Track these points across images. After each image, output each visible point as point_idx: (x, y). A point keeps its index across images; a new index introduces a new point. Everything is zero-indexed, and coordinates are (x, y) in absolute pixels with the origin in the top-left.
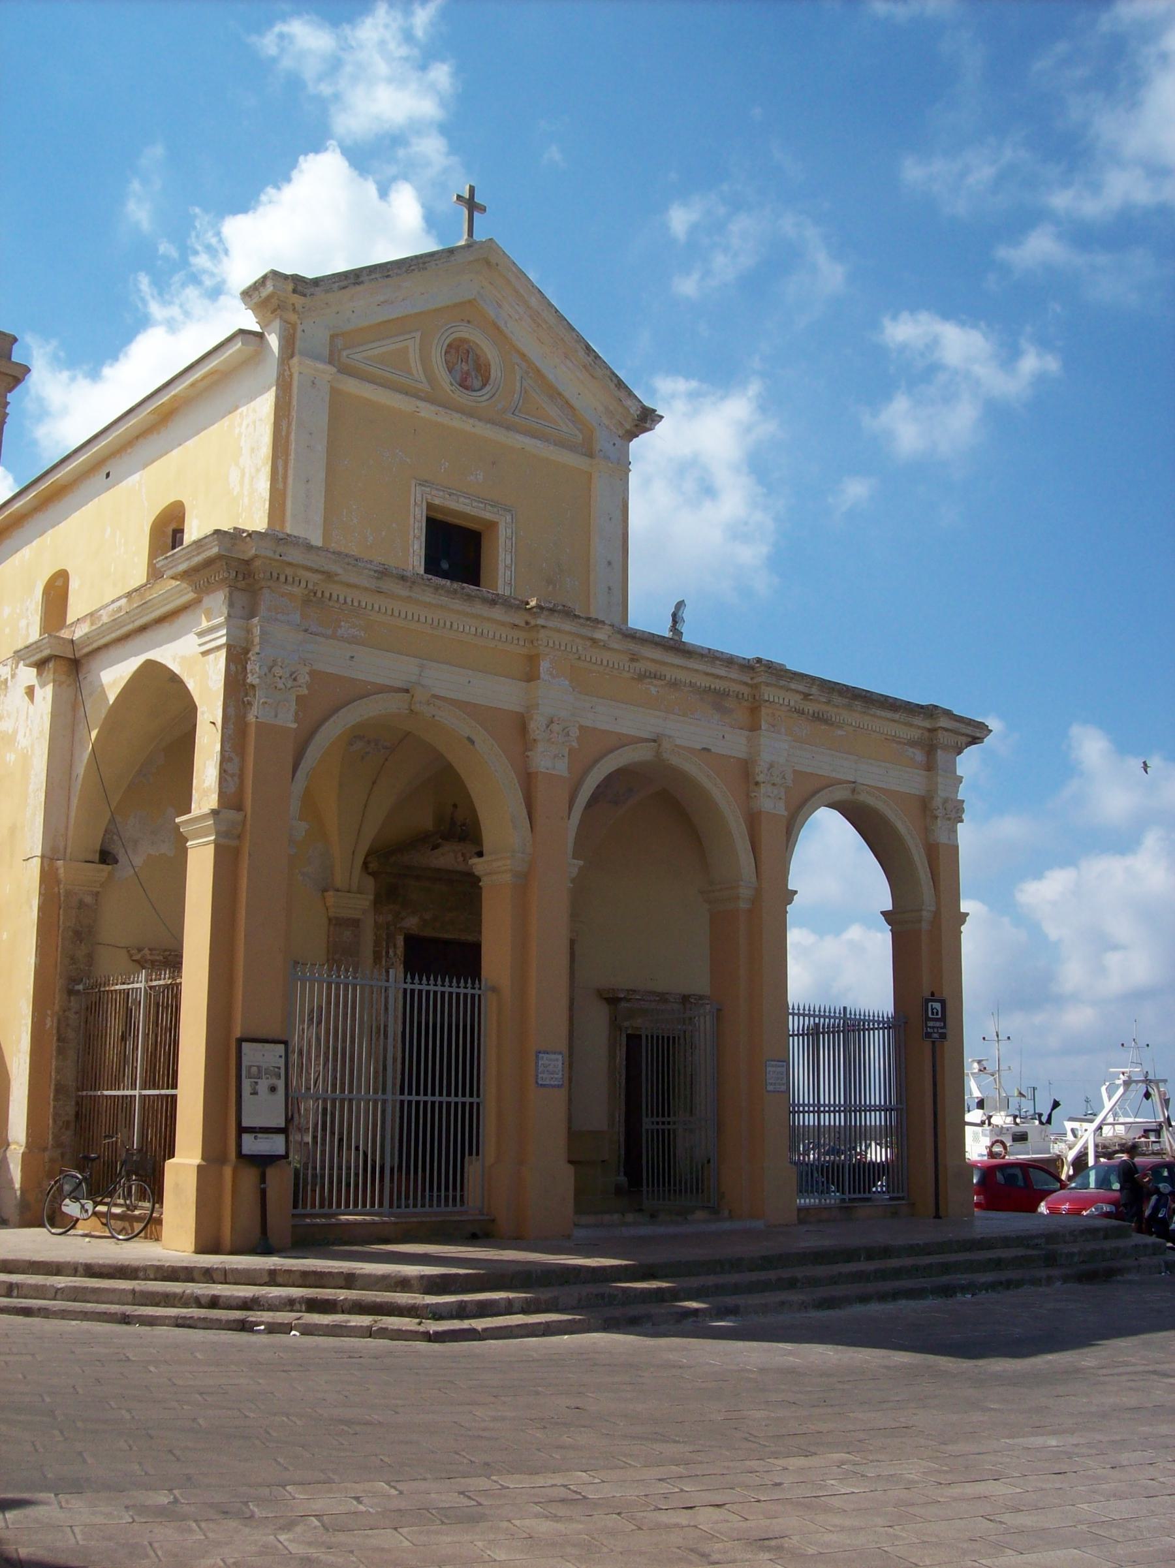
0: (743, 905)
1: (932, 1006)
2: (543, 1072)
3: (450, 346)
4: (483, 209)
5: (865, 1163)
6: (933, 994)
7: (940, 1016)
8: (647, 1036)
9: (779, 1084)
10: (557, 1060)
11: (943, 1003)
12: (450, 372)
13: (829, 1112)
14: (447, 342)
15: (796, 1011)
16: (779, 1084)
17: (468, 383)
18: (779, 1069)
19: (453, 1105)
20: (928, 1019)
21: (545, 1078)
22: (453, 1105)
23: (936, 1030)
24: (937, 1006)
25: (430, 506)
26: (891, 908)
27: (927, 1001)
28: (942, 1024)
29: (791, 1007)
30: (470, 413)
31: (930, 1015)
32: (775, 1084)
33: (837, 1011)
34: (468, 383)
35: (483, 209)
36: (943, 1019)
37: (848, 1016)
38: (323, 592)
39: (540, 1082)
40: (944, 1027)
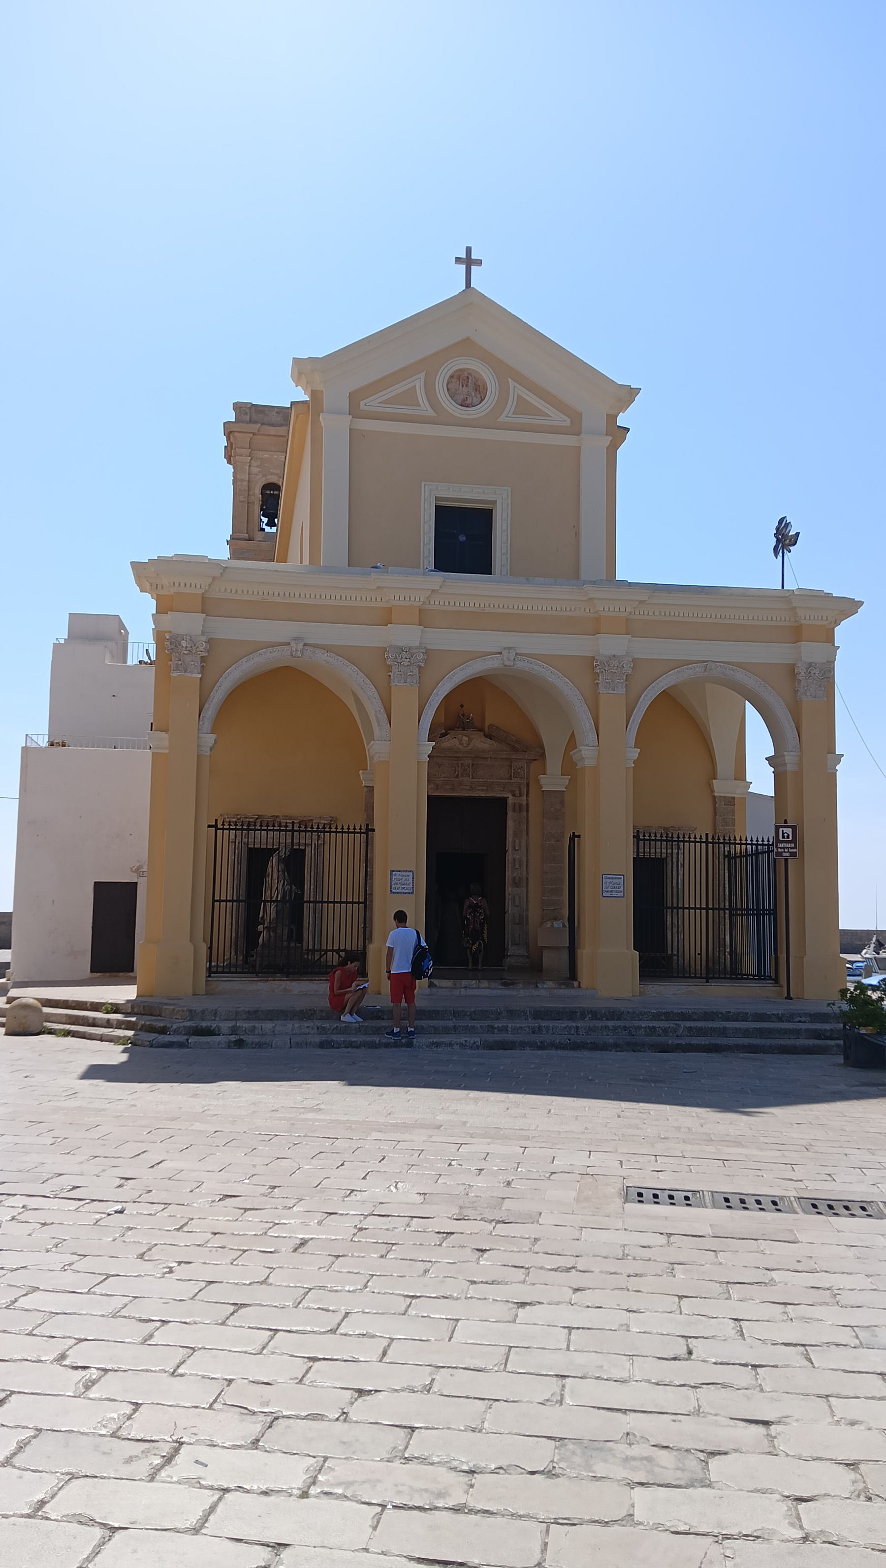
0: (588, 763)
1: (783, 831)
2: (397, 884)
3: (452, 377)
4: (479, 263)
6: (786, 822)
7: (791, 839)
9: (619, 892)
13: (742, 915)
16: (619, 892)
24: (789, 831)
25: (437, 499)
26: (773, 754)
31: (781, 838)
32: (611, 891)
35: (479, 263)
38: (822, 616)
39: (393, 891)
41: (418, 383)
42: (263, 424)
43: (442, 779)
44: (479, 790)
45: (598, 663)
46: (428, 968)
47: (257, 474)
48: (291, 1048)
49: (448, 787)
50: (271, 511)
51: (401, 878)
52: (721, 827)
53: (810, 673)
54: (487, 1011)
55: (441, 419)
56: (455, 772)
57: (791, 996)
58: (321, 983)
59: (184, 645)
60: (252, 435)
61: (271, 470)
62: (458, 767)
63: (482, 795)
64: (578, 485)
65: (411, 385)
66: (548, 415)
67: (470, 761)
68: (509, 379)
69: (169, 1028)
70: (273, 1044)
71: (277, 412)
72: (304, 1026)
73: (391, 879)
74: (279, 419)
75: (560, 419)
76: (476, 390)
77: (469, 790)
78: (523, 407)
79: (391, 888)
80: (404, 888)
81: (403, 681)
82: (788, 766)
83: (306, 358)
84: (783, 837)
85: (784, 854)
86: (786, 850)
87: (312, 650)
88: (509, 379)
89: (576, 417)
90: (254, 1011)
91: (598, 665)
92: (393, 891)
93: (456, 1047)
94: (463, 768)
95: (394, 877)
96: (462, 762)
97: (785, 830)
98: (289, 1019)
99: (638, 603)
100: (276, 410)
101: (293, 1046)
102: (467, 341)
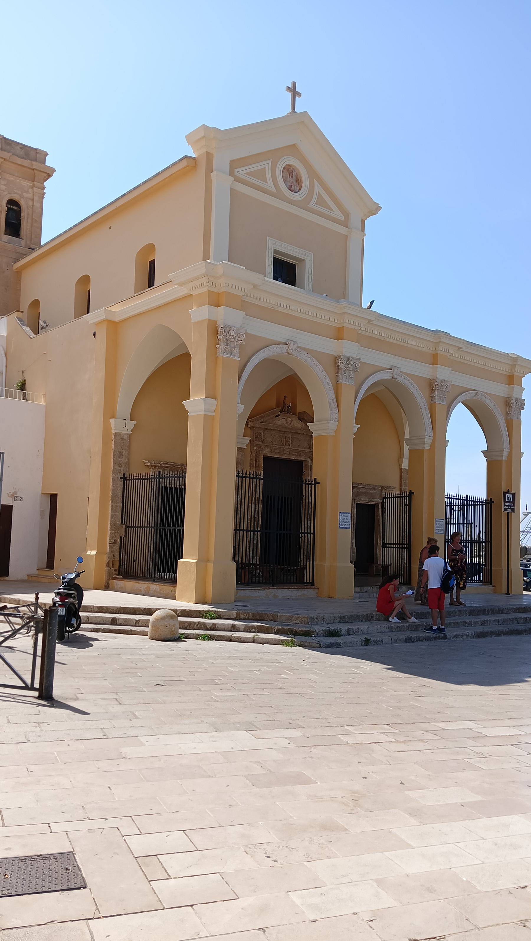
0: (427, 447)
1: (508, 496)
3: (284, 168)
5: (173, 572)
6: (508, 490)
7: (512, 501)
8: (279, 497)
9: (441, 530)
10: (348, 516)
11: (513, 494)
12: (285, 182)
14: (283, 167)
15: (478, 500)
16: (441, 530)
17: (292, 188)
18: (440, 523)
19: (282, 534)
20: (506, 502)
21: (343, 525)
22: (282, 534)
23: (509, 507)
24: (511, 496)
25: (275, 251)
26: (487, 450)
27: (506, 493)
28: (513, 505)
29: (446, 495)
30: (292, 202)
31: (507, 500)
32: (439, 530)
33: (464, 497)
34: (292, 188)
36: (513, 502)
37: (469, 499)
39: (340, 526)
40: (514, 506)
41: (267, 166)
42: (14, 154)
43: (275, 446)
44: (293, 455)
45: (438, 384)
46: (453, 585)
47: (4, 191)
48: (392, 643)
49: (278, 451)
50: (13, 221)
51: (344, 517)
52: (404, 488)
53: (516, 403)
54: (450, 611)
55: (278, 195)
56: (281, 442)
57: (509, 593)
58: (293, 591)
59: (232, 335)
60: (3, 160)
61: (14, 190)
62: (284, 438)
63: (296, 459)
64: (346, 261)
65: (262, 167)
66: (332, 210)
67: (290, 435)
68: (314, 180)
69: (313, 632)
70: (383, 641)
71: (20, 148)
72: (382, 627)
73: (339, 519)
74: (21, 153)
75: (338, 214)
76: (297, 182)
77: (288, 454)
78: (321, 202)
79: (339, 525)
80: (346, 525)
81: (347, 381)
82: (503, 457)
83: (211, 127)
84: (508, 499)
85: (508, 510)
86: (509, 507)
87: (299, 350)
88: (314, 180)
89: (347, 215)
90: (344, 616)
91: (437, 385)
92: (340, 526)
93: (464, 637)
94: (286, 439)
95: (341, 517)
96: (286, 435)
97: (509, 495)
98: (360, 621)
99: (457, 349)
100: (20, 146)
101: (393, 642)
102: (293, 146)
